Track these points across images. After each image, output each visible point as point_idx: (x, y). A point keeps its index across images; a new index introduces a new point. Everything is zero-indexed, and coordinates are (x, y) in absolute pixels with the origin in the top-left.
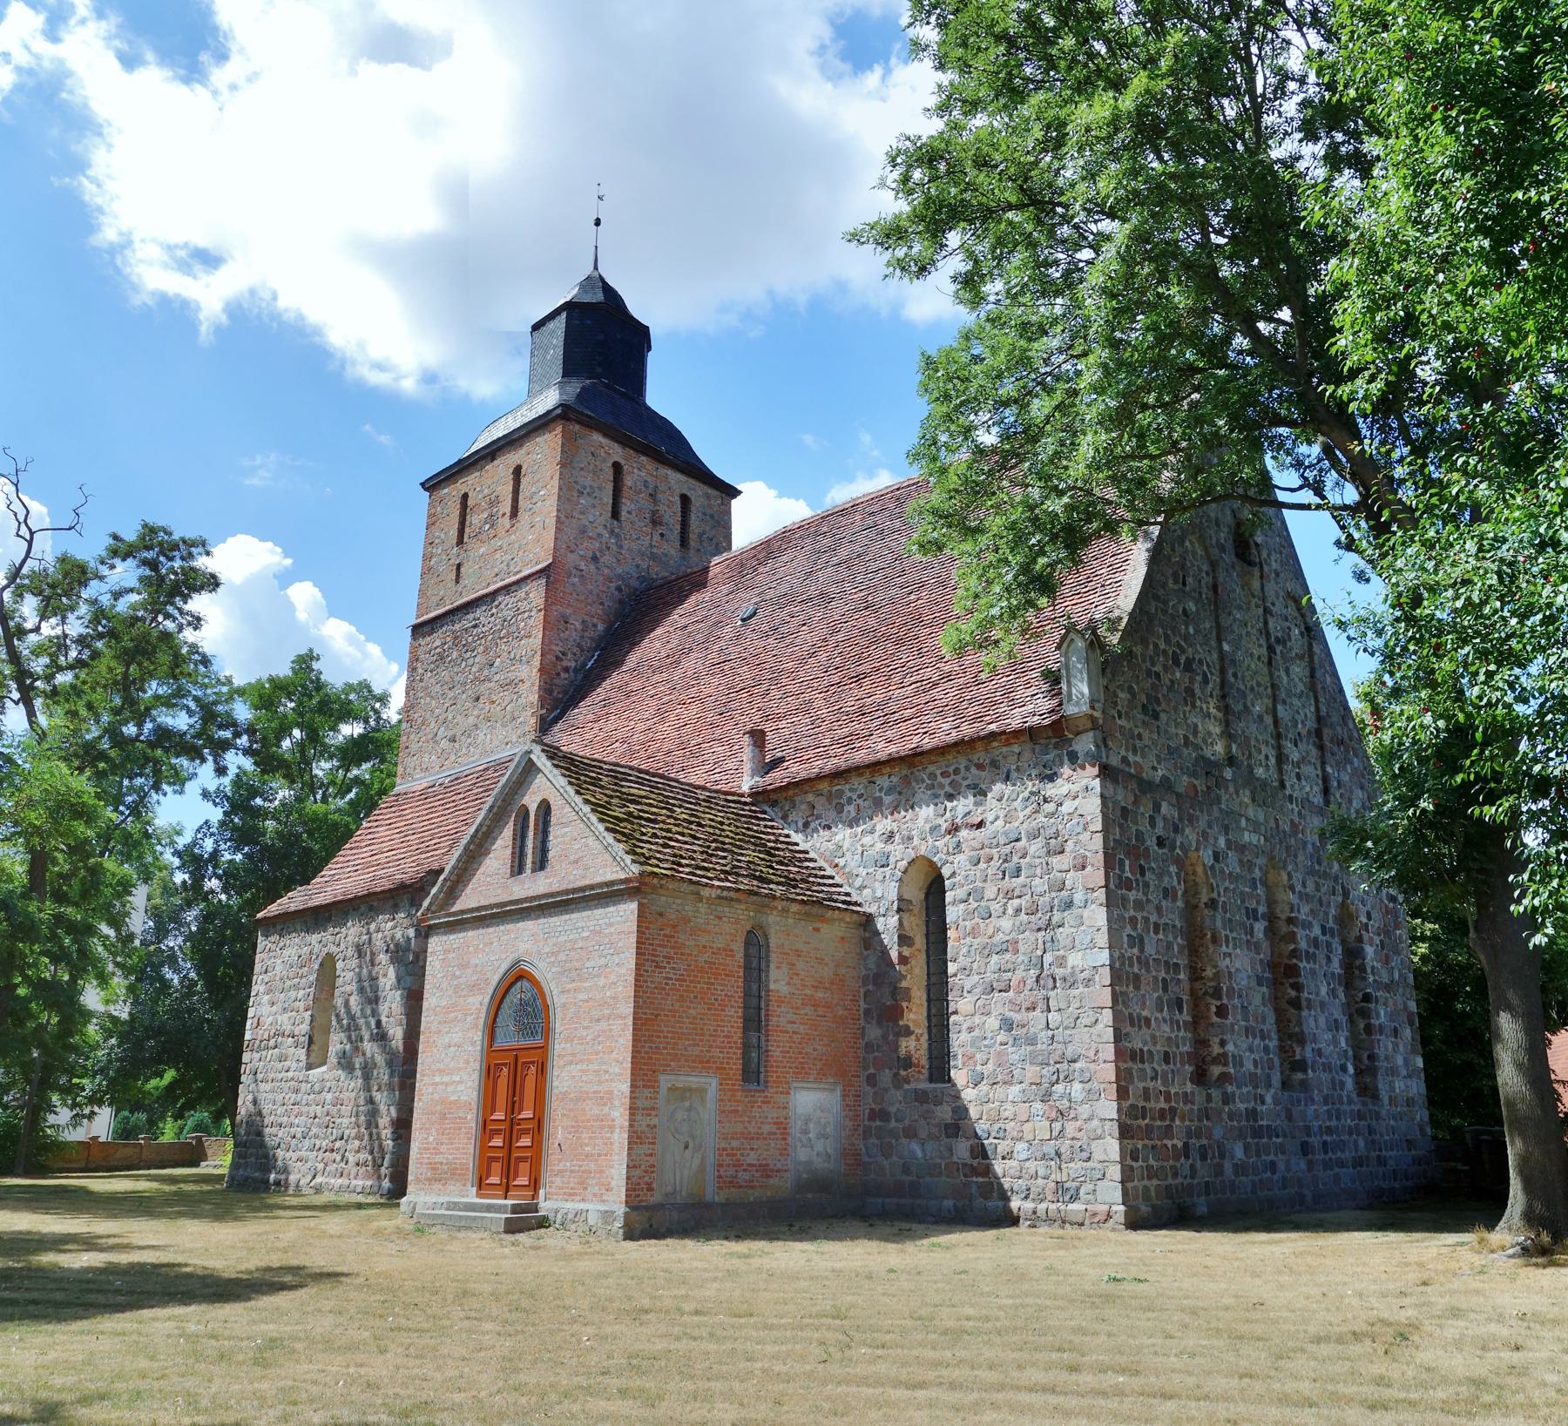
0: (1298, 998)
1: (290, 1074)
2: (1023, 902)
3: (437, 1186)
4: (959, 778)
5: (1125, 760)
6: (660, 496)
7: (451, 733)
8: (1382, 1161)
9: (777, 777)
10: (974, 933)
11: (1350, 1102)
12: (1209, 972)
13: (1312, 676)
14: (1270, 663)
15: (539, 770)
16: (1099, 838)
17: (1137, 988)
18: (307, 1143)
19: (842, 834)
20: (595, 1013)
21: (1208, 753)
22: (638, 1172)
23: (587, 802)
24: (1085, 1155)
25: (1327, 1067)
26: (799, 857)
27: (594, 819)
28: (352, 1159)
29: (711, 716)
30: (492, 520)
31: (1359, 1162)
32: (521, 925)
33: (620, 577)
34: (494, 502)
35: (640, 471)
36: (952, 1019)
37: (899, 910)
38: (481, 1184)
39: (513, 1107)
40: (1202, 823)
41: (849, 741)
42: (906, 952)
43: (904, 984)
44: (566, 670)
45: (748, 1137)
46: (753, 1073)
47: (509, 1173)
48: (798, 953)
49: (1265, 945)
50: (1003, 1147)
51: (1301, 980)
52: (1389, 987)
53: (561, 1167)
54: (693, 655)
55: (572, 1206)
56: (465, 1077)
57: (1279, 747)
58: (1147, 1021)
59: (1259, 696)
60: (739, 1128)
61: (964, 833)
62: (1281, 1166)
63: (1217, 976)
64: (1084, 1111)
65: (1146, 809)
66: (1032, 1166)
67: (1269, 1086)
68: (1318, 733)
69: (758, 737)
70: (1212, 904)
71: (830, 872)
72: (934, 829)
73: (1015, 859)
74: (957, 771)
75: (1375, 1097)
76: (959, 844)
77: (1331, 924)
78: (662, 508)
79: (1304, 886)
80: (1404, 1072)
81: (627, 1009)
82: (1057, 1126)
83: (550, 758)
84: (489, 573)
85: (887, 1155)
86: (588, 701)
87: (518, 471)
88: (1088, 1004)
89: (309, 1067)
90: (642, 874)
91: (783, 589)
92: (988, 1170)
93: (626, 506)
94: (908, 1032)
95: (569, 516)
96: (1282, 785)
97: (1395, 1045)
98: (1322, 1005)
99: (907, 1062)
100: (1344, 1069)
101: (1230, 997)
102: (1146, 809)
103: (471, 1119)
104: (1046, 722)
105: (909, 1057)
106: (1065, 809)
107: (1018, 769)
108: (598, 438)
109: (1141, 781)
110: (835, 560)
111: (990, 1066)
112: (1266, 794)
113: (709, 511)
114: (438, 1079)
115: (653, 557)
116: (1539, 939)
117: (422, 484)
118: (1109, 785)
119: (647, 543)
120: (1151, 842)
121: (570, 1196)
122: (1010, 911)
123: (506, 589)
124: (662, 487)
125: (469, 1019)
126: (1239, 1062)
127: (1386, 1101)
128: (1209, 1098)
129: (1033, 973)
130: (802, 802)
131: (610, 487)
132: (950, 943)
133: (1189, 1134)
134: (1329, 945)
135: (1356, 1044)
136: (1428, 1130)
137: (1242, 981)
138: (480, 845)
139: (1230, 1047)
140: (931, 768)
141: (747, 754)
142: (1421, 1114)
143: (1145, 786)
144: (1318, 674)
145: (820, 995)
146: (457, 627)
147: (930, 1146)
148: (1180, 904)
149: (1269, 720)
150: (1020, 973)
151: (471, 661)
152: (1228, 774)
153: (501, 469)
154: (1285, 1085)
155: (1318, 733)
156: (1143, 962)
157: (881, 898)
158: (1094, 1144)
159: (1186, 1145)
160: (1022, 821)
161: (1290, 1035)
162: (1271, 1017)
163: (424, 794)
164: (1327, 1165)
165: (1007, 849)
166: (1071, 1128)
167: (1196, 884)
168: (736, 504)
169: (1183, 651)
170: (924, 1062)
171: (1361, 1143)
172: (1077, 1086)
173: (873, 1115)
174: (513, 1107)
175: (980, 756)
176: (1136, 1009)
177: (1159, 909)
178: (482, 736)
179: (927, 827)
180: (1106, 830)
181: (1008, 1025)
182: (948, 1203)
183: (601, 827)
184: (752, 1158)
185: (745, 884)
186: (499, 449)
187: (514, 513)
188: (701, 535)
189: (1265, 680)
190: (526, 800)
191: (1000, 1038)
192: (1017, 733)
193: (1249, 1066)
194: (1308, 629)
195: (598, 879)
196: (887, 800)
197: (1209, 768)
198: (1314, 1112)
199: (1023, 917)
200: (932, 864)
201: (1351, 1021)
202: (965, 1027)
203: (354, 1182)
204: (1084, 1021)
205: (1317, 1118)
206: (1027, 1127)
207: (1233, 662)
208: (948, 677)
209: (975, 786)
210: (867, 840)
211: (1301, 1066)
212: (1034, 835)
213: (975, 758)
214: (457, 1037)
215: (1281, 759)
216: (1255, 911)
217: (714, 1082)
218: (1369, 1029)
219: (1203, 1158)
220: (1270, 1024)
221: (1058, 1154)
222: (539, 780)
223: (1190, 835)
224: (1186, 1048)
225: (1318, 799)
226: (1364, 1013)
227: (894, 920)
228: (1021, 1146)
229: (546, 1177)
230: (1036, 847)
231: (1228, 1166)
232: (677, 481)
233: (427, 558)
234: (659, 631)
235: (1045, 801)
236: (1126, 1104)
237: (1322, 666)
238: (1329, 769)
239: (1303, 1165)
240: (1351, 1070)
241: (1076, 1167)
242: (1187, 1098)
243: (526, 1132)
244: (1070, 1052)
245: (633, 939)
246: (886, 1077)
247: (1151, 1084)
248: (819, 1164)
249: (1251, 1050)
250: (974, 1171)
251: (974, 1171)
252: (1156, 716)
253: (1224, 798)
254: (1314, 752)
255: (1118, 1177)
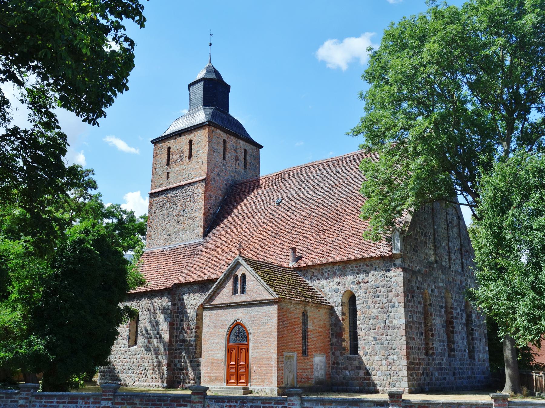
0: (453, 331)
1: (122, 349)
2: (380, 305)
3: (211, 383)
4: (360, 268)
5: (409, 266)
6: (238, 150)
7: (168, 233)
8: (475, 378)
9: (301, 263)
10: (365, 313)
11: (467, 360)
12: (429, 324)
13: (459, 231)
14: (447, 230)
15: (241, 265)
16: (402, 289)
17: (411, 330)
18: (130, 371)
19: (323, 282)
20: (265, 336)
21: (430, 260)
22: (280, 378)
23: (259, 276)
24: (397, 375)
25: (461, 351)
26: (310, 289)
27: (262, 281)
28: (150, 376)
29: (271, 238)
30: (181, 158)
31: (468, 378)
32: (237, 309)
33: (226, 180)
34: (181, 152)
35: (232, 142)
36: (358, 337)
37: (342, 305)
38: (228, 382)
39: (238, 360)
40: (428, 282)
41: (324, 253)
42: (344, 317)
43: (343, 327)
44: (211, 214)
45: (304, 369)
46: (305, 353)
47: (238, 379)
48: (315, 318)
49: (444, 316)
50: (374, 373)
51: (454, 325)
52: (479, 326)
53: (255, 377)
54: (260, 214)
55: (260, 388)
56: (220, 352)
57: (449, 256)
58: (414, 338)
59: (444, 240)
60: (302, 367)
61: (362, 284)
62: (447, 379)
63: (432, 325)
64: (397, 363)
65: (414, 279)
66: (382, 378)
67: (445, 356)
68: (461, 249)
69: (294, 250)
70: (431, 305)
71: (319, 293)
72: (353, 282)
73: (378, 293)
74: (360, 266)
75: (474, 359)
76: (360, 287)
77: (463, 308)
78: (238, 154)
79: (456, 297)
80: (482, 352)
81: (276, 335)
82: (390, 367)
83: (246, 261)
84: (181, 178)
85: (338, 375)
86: (221, 226)
87: (191, 142)
88: (398, 334)
89: (129, 347)
90: (279, 298)
91: (290, 194)
92: (369, 379)
93: (228, 155)
94: (344, 340)
95: (211, 160)
96: (450, 267)
97: (480, 343)
98: (460, 332)
99: (344, 349)
100: (465, 351)
101: (435, 331)
102: (414, 279)
103: (223, 364)
104: (388, 255)
105: (345, 347)
106: (393, 279)
107: (379, 267)
108: (219, 131)
109: (412, 270)
110: (308, 186)
111: (370, 350)
112: (445, 270)
113: (253, 154)
114: (210, 353)
115: (236, 172)
116: (501, 341)
117: (151, 141)
118: (405, 274)
119: (234, 167)
120: (415, 289)
121: (259, 385)
122: (376, 307)
123: (189, 184)
124: (238, 147)
125: (220, 336)
126: (437, 350)
127: (477, 360)
128: (429, 359)
129: (383, 325)
130: (310, 271)
131: (222, 148)
132: (358, 316)
133: (424, 369)
134: (462, 314)
135: (469, 343)
136: (489, 369)
137: (438, 326)
138: (221, 285)
139: (435, 345)
140: (352, 265)
141: (291, 254)
142: (487, 364)
143: (414, 272)
144: (461, 231)
145: (320, 329)
146: (169, 195)
147: (352, 372)
148: (422, 305)
149: (447, 247)
150: (379, 325)
151: (175, 208)
152: (435, 266)
153: (184, 141)
154: (449, 356)
155: (461, 249)
156: (413, 323)
157: (336, 300)
158: (400, 372)
159: (423, 372)
160: (380, 282)
161: (451, 341)
162: (446, 336)
163: (160, 254)
164: (460, 379)
165: (375, 290)
166: (393, 367)
167: (426, 299)
168: (261, 151)
169: (424, 230)
170: (349, 349)
171: (470, 373)
172: (395, 356)
173: (334, 363)
174: (238, 360)
175: (367, 262)
176: (411, 335)
177: (417, 307)
178: (181, 235)
179: (351, 282)
180: (404, 286)
181: (375, 339)
182: (357, 388)
183: (265, 284)
184: (305, 375)
185: (302, 299)
186: (183, 133)
187: (190, 157)
188: (250, 163)
189: (446, 235)
190: (237, 273)
191: (373, 343)
192: (378, 257)
193: (439, 350)
194: (459, 217)
195: (264, 298)
196: (338, 273)
197: (430, 265)
198: (457, 363)
199: (380, 309)
200: (351, 292)
201: (468, 337)
202: (362, 339)
203: (151, 384)
204: (397, 339)
205: (457, 365)
206: (381, 367)
207: (437, 231)
208: (354, 235)
209: (365, 271)
210: (332, 284)
211: (453, 350)
212: (383, 286)
213: (366, 263)
214: (216, 340)
215: (450, 259)
216: (442, 306)
217: (296, 354)
218: (473, 339)
219: (427, 376)
220: (445, 339)
221: (390, 375)
222: (241, 267)
223: (425, 285)
224: (423, 346)
225: (460, 270)
226: (472, 334)
227: (340, 308)
228: (379, 372)
229: (250, 380)
230: (384, 290)
231: (434, 378)
232: (243, 144)
233: (154, 168)
234: (244, 203)
235: (387, 277)
236: (409, 361)
237: (462, 228)
238: (464, 261)
239: (453, 378)
240: (467, 351)
241: (395, 378)
242: (423, 360)
243: (243, 368)
244: (393, 347)
245: (276, 315)
246: (338, 353)
247: (415, 356)
248: (321, 377)
249: (440, 346)
250: (365, 379)
251: (365, 379)
252: (417, 252)
253: (434, 273)
254: (459, 255)
255: (407, 380)
